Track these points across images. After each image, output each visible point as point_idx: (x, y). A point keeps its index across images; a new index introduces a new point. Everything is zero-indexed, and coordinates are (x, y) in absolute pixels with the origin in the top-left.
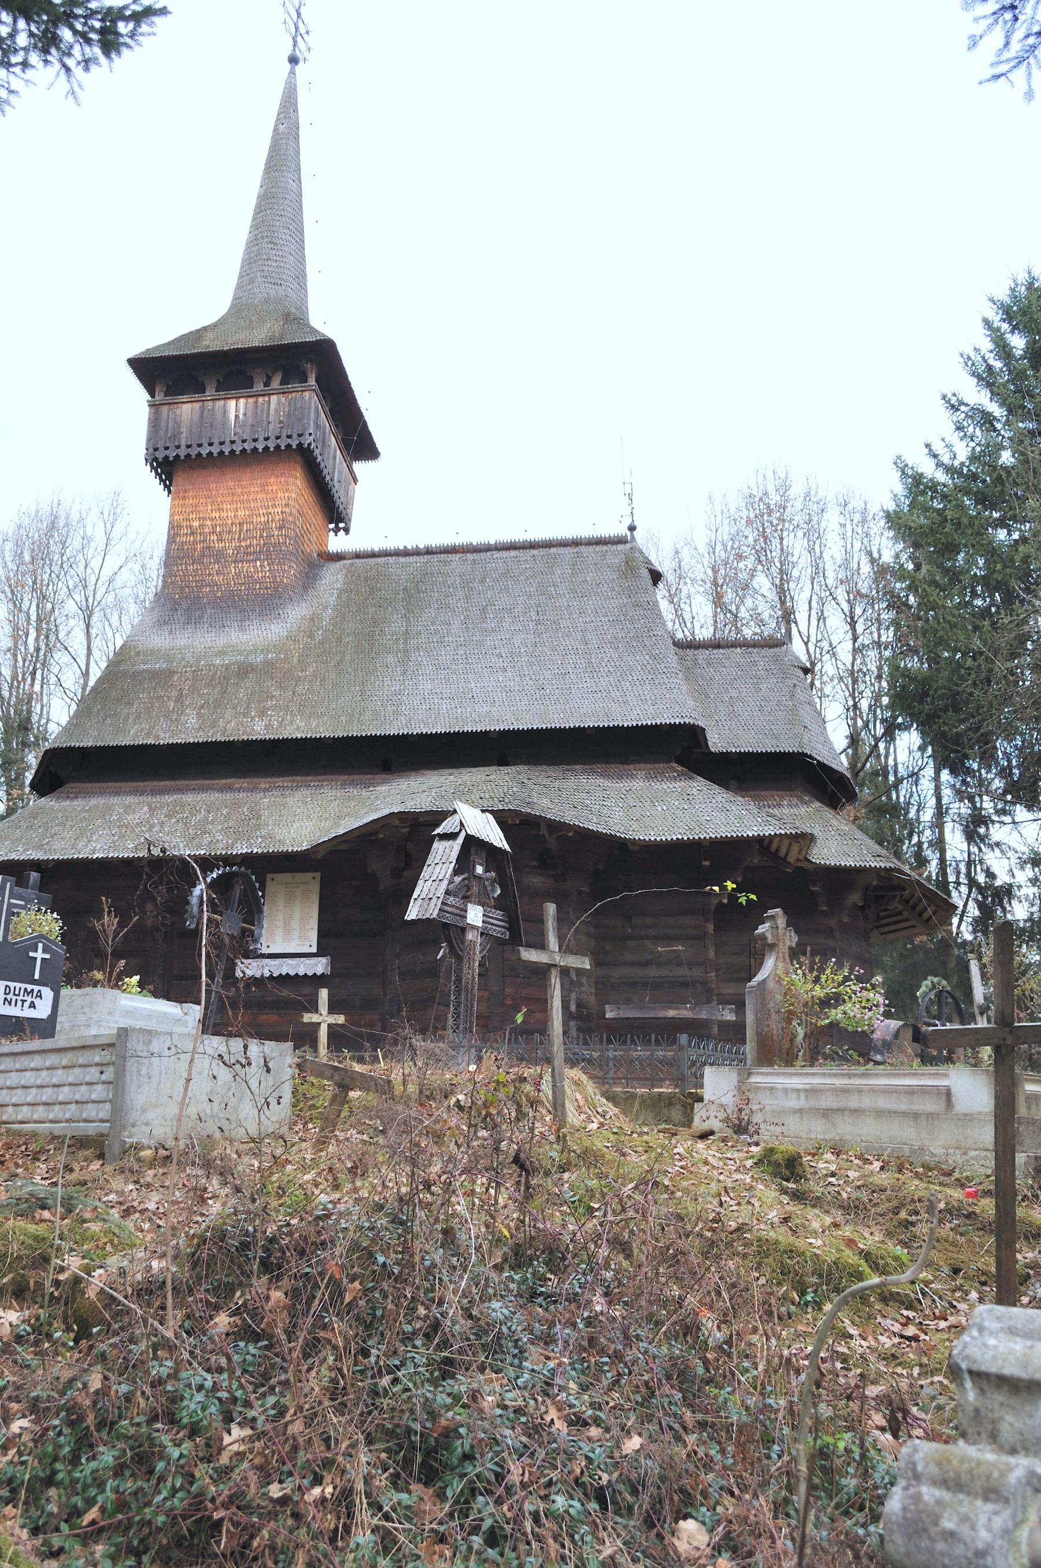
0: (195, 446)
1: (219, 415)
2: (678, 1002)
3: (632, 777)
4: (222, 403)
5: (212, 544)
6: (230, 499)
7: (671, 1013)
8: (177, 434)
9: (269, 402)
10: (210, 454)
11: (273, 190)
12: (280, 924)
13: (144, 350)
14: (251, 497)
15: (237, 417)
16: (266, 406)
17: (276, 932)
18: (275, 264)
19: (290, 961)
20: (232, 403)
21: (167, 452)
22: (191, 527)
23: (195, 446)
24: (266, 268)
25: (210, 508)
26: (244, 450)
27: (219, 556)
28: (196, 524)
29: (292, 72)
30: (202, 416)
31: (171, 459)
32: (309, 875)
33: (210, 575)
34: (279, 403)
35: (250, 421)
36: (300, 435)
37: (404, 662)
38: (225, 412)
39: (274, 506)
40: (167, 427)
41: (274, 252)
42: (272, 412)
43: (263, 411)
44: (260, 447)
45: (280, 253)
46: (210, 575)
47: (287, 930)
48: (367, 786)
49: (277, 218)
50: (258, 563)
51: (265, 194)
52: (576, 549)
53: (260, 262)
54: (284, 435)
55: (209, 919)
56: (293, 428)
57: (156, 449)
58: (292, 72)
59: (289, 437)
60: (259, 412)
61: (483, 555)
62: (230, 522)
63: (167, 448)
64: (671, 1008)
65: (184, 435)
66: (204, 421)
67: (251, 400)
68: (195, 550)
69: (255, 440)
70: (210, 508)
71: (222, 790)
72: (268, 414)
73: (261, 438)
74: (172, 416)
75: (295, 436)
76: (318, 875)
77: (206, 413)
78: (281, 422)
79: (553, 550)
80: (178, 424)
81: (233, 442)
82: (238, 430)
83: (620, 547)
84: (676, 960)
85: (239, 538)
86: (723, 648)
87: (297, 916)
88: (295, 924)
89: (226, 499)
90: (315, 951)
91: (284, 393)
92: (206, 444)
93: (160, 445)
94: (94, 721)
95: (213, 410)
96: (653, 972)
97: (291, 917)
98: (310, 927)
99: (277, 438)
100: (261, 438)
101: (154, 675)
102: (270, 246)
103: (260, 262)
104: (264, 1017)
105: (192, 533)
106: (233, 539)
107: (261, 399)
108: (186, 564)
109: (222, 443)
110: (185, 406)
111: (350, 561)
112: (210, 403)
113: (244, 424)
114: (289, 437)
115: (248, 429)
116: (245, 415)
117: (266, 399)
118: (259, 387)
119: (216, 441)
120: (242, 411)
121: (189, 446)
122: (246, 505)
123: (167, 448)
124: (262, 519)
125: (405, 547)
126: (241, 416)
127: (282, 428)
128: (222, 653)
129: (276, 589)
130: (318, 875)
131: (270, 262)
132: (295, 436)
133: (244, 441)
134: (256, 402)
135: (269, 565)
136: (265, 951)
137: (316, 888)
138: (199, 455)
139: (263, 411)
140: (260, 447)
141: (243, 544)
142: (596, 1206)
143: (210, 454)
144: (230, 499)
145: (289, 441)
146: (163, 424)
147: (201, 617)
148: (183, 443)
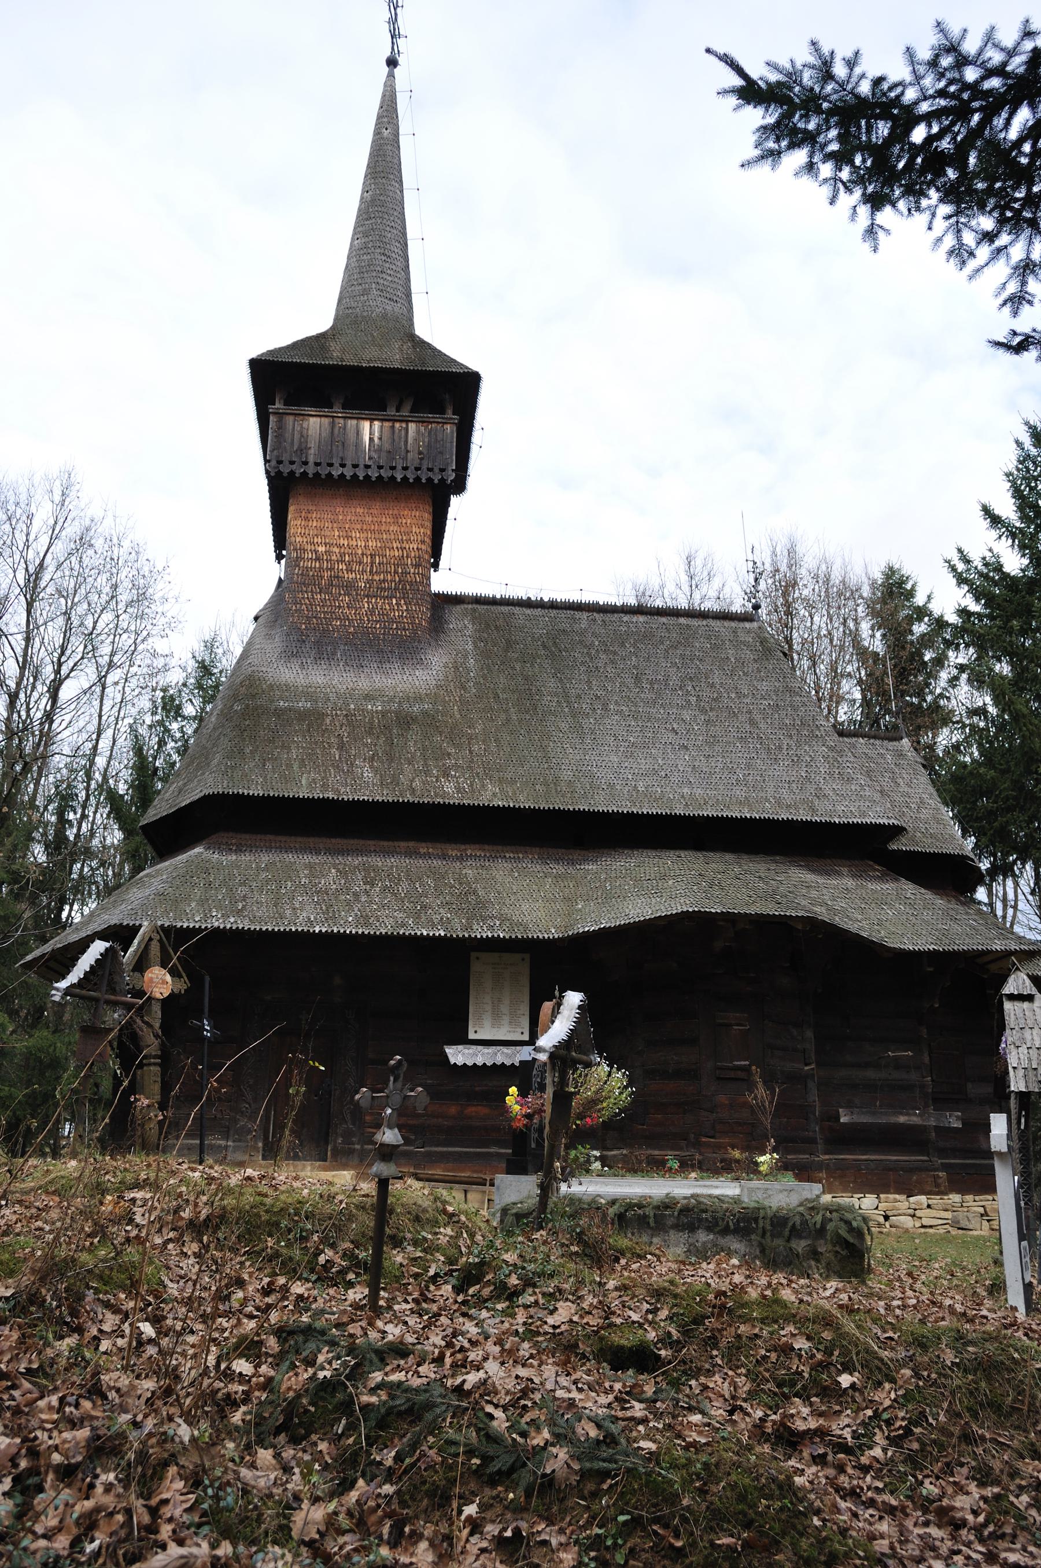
0: (324, 465)
1: (351, 435)
2: (903, 1107)
3: (839, 874)
4: (354, 422)
5: (340, 574)
6: (359, 527)
7: (902, 1119)
8: (303, 449)
9: (407, 429)
10: (342, 476)
11: (381, 198)
12: (488, 1007)
13: (264, 350)
14: (383, 528)
15: (371, 439)
16: (403, 432)
17: (484, 1017)
18: (389, 278)
19: (505, 1050)
20: (366, 425)
21: (294, 467)
22: (316, 552)
23: (324, 465)
24: (381, 281)
25: (337, 533)
26: (380, 477)
27: (350, 587)
28: (322, 549)
29: (391, 75)
30: (332, 432)
31: (285, 475)
32: (518, 956)
33: (339, 607)
34: (418, 432)
35: (387, 446)
36: (442, 470)
37: (578, 729)
38: (358, 433)
39: (409, 541)
40: (293, 440)
41: (387, 265)
42: (410, 440)
43: (400, 438)
44: (399, 477)
45: (394, 267)
46: (339, 607)
47: (497, 1017)
48: (572, 862)
49: (388, 229)
50: (394, 601)
51: (373, 200)
52: (704, 623)
53: (374, 274)
54: (424, 467)
55: (174, 964)
56: (434, 461)
57: (280, 462)
58: (391, 75)
59: (430, 470)
60: (396, 437)
61: (609, 617)
62: (360, 552)
63: (292, 463)
64: (902, 1114)
65: (312, 451)
66: (335, 440)
67: (387, 424)
68: (322, 577)
69: (393, 468)
70: (337, 533)
71: (409, 854)
72: (406, 441)
73: (399, 467)
74: (298, 428)
75: (436, 470)
76: (527, 956)
77: (336, 431)
78: (420, 453)
79: (682, 620)
80: (304, 437)
81: (367, 467)
82: (374, 455)
83: (747, 625)
84: (898, 1064)
85: (371, 571)
86: (847, 736)
87: (506, 1001)
88: (505, 1008)
89: (353, 526)
90: (527, 1039)
91: (423, 422)
92: (337, 465)
93: (285, 458)
94: (252, 765)
95: (345, 428)
96: (871, 1074)
97: (500, 1000)
98: (521, 1012)
99: (417, 469)
100: (399, 467)
101: (303, 716)
102: (384, 258)
103: (374, 274)
104: (473, 1109)
105: (317, 559)
106: (364, 571)
107: (397, 425)
108: (312, 591)
109: (355, 466)
110: (312, 420)
111: (470, 606)
112: (342, 421)
113: (380, 450)
114: (430, 470)
115: (384, 455)
116: (380, 439)
117: (404, 425)
118: (391, 412)
119: (349, 463)
120: (377, 434)
121: (317, 464)
122: (377, 536)
123: (292, 463)
124: (397, 554)
125: (529, 598)
126: (376, 440)
127: (421, 459)
128: (368, 697)
129: (415, 632)
130: (527, 956)
131: (384, 275)
132: (436, 470)
133: (380, 467)
134: (393, 427)
135: (405, 604)
136: (472, 1036)
137: (526, 971)
138: (330, 475)
139: (400, 438)
140: (399, 477)
141: (376, 578)
142: (138, 1219)
143: (342, 476)
144: (359, 527)
145: (430, 474)
146: (288, 436)
147: (334, 654)
148: (311, 460)
